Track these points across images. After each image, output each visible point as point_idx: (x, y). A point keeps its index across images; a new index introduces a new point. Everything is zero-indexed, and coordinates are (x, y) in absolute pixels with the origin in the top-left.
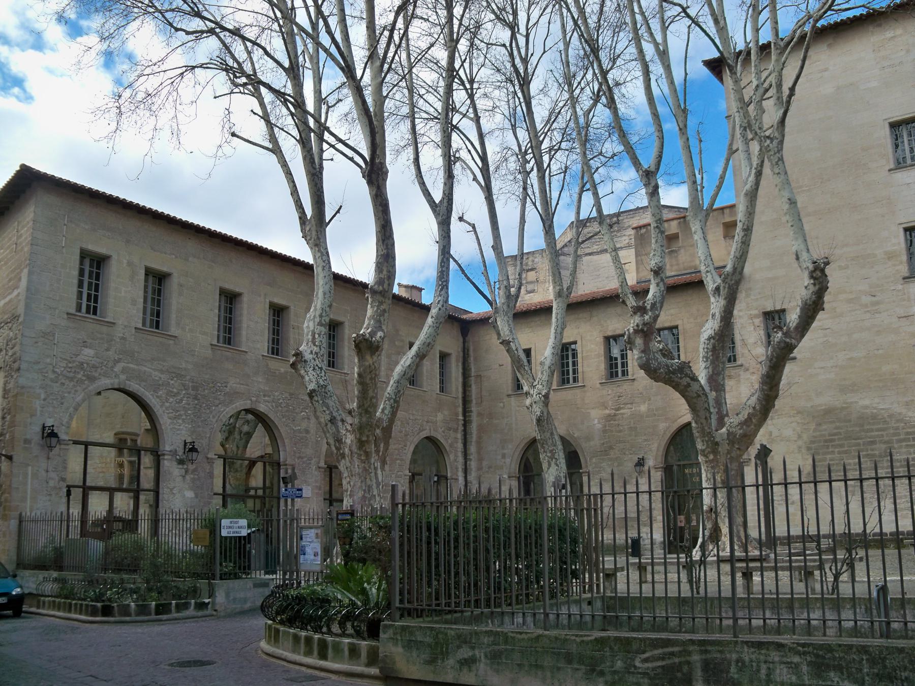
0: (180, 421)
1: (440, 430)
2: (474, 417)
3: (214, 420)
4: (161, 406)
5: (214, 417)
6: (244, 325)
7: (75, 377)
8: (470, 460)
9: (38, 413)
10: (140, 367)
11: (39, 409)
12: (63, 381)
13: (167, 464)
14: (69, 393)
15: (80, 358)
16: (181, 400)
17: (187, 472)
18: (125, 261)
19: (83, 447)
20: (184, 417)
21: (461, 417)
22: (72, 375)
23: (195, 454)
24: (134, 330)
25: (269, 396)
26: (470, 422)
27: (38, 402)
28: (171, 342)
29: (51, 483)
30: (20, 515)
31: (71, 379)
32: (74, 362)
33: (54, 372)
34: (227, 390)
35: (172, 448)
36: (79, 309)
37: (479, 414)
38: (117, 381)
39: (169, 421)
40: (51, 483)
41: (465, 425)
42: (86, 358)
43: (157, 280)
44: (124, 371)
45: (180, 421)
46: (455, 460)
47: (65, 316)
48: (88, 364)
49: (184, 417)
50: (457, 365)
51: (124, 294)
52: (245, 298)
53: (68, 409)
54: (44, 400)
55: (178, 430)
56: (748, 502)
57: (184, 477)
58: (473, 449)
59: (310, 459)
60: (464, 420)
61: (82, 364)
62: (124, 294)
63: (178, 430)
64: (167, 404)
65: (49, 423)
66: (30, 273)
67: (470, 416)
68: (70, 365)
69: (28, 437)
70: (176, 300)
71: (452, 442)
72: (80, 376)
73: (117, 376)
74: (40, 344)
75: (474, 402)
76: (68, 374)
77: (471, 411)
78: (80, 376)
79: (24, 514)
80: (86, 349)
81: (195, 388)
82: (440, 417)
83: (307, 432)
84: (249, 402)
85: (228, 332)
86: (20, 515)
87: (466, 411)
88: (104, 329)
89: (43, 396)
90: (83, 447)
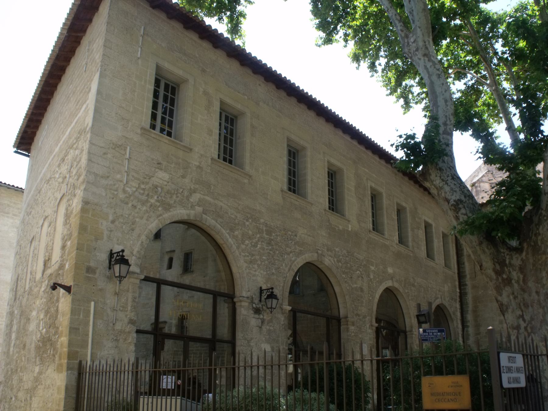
0: (256, 266)
1: (447, 299)
2: (469, 290)
3: (287, 269)
4: (238, 248)
5: (286, 266)
6: (309, 178)
7: (147, 201)
8: (468, 327)
9: (105, 238)
10: (216, 202)
11: (106, 233)
12: (135, 203)
13: (244, 311)
14: (142, 218)
15: (155, 180)
16: (257, 243)
17: (263, 322)
18: (201, 90)
19: (155, 285)
20: (259, 262)
21: (458, 290)
22: (144, 198)
23: (275, 301)
24: (210, 161)
25: (331, 251)
26: (466, 294)
27: (105, 223)
28: (246, 181)
29: (118, 326)
30: (80, 362)
31: (143, 203)
32: (147, 183)
33: (124, 191)
34: (297, 239)
35: (249, 294)
36: (153, 127)
37: (474, 287)
38: (193, 212)
39: (245, 265)
40: (118, 326)
41: (461, 297)
42: (161, 182)
43: (229, 122)
44: (200, 203)
45: (256, 266)
46: (457, 326)
47: (139, 131)
48: (162, 188)
49: (259, 262)
50: (453, 246)
51: (199, 123)
52: (309, 153)
53: (139, 236)
54: (113, 222)
55: (254, 275)
56: (249, 381)
57: (260, 328)
58: (469, 317)
59: (365, 317)
60: (460, 293)
61: (156, 187)
62: (199, 123)
63: (254, 275)
64: (243, 246)
65: (117, 248)
66: (101, 76)
67: (465, 289)
68: (143, 186)
69: (92, 264)
70: (249, 142)
71: (454, 309)
72: (152, 201)
73: (192, 207)
74: (109, 156)
75: (468, 276)
76: (140, 197)
77: (466, 285)
78: (152, 201)
79: (84, 363)
80: (160, 172)
81: (269, 233)
82: (446, 288)
83: (362, 290)
84: (316, 254)
85: (294, 184)
86: (80, 362)
87: (462, 285)
88: (181, 153)
89: (111, 218)
90: (155, 285)
